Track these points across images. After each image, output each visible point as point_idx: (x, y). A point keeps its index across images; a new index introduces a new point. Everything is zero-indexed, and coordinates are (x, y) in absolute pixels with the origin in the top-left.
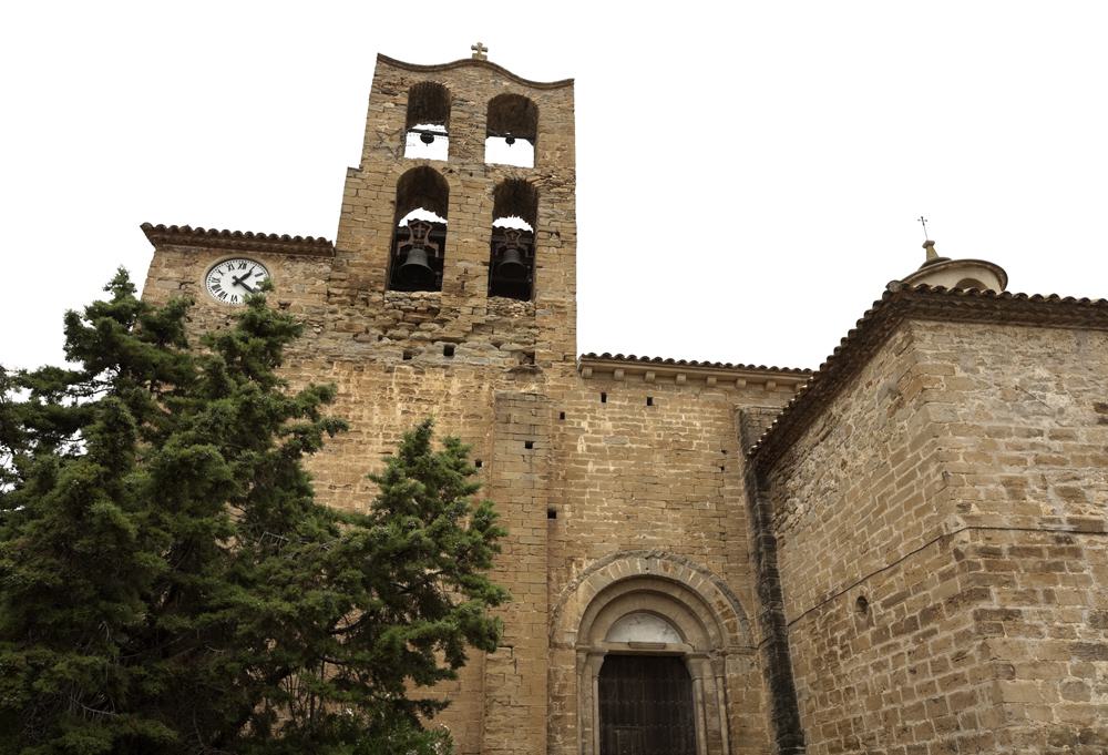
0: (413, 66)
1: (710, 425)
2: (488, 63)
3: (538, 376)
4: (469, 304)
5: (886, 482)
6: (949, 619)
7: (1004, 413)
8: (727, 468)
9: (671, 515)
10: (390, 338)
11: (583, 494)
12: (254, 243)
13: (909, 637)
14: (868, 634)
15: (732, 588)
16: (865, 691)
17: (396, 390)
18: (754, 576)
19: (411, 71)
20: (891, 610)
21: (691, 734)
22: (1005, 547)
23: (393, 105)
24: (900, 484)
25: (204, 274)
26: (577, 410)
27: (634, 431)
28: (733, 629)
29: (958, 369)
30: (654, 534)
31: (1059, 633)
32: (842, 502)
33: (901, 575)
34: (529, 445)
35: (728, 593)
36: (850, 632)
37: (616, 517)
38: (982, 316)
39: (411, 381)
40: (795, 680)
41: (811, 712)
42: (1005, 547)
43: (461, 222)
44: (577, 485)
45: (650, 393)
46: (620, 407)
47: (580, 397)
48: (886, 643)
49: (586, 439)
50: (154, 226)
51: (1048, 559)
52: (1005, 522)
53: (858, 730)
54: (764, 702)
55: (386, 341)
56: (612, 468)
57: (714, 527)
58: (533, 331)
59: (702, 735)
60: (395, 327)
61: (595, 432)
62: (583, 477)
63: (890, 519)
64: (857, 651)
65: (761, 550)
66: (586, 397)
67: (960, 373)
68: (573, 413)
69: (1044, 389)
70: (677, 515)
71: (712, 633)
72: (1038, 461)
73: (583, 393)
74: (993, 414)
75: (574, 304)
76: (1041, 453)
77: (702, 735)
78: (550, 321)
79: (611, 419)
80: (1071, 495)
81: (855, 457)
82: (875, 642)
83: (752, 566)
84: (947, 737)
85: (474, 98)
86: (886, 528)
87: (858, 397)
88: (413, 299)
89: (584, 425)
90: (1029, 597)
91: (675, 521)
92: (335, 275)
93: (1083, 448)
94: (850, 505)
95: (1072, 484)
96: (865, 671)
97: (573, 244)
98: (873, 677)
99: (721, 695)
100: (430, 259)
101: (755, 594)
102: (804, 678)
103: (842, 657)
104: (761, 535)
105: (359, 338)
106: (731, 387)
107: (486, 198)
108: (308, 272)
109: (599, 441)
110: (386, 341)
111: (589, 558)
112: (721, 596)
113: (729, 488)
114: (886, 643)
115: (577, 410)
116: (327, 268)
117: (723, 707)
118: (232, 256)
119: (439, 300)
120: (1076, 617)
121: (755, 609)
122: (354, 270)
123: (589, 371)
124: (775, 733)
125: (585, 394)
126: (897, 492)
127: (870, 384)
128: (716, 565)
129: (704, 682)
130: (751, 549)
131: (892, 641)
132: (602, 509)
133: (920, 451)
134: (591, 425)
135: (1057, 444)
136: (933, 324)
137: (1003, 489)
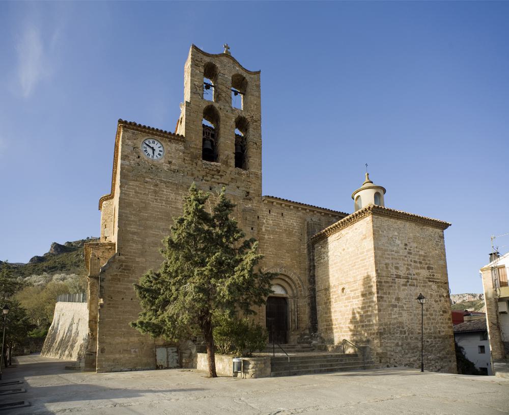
0: (206, 53)
1: (298, 225)
2: (231, 56)
3: (251, 201)
4: (229, 170)
5: (357, 259)
6: (368, 297)
7: (388, 245)
8: (302, 240)
9: (287, 255)
10: (206, 181)
11: (264, 246)
12: (158, 133)
13: (357, 300)
14: (344, 297)
15: (302, 279)
16: (341, 312)
17: (209, 202)
18: (307, 276)
19: (205, 55)
20: (353, 292)
21: (92, 306)
22: (383, 281)
23: (199, 72)
24: (361, 260)
25: (141, 144)
26: (262, 216)
27: (278, 225)
28: (301, 291)
29: (380, 231)
30: (282, 260)
31: (389, 302)
32: (342, 261)
33: (357, 284)
34: (252, 229)
35: (300, 280)
36: (338, 297)
37: (273, 254)
38: (387, 216)
39: (214, 199)
40: (317, 307)
41: (321, 316)
42: (383, 281)
43: (225, 133)
44: (263, 243)
45: (282, 211)
46: (275, 216)
47: (263, 211)
48: (349, 301)
49: (265, 227)
50: (123, 120)
51: (390, 284)
52: (384, 275)
53: (336, 321)
54: (307, 312)
55: (204, 181)
56: (272, 237)
57: (298, 259)
58: (249, 183)
59: (290, 320)
60: (206, 176)
61: (267, 224)
62: (264, 240)
63: (356, 269)
64: (340, 301)
65: (311, 268)
66: (265, 211)
67: (381, 233)
68: (261, 217)
69: (396, 238)
70: (289, 255)
71: (295, 292)
72: (392, 258)
73: (264, 209)
74: (386, 245)
75: (261, 174)
76: (393, 257)
77: (290, 320)
78: (254, 180)
79: (272, 220)
80: (397, 268)
81: (348, 249)
82: (346, 300)
83: (307, 272)
84: (362, 324)
85: (226, 73)
86: (355, 271)
87: (352, 231)
88: (211, 165)
89: (264, 221)
90: (385, 293)
91: (288, 256)
92: (186, 151)
93: (401, 256)
94: (344, 262)
95: (397, 265)
96: (342, 307)
97: (261, 149)
98: (343, 309)
99: (296, 310)
100: (212, 145)
101: (307, 281)
102: (320, 307)
103: (335, 302)
104: (312, 264)
105: (195, 179)
106: (304, 212)
107: (232, 122)
108: (177, 148)
109: (268, 227)
110: (204, 181)
111: (266, 267)
112: (299, 282)
113: (302, 247)
114: (349, 301)
115: (262, 216)
116: (182, 148)
117: (296, 313)
118: (150, 137)
119: (220, 167)
120: (393, 298)
121: (307, 285)
122: (192, 150)
123: (266, 202)
124: (310, 321)
125: (264, 208)
126: (360, 262)
127: (356, 229)
128: (297, 271)
129: (291, 305)
130: (307, 267)
131: (351, 300)
132: (269, 251)
133: (368, 253)
134: (266, 221)
135: (396, 254)
136: (377, 217)
137: (385, 266)
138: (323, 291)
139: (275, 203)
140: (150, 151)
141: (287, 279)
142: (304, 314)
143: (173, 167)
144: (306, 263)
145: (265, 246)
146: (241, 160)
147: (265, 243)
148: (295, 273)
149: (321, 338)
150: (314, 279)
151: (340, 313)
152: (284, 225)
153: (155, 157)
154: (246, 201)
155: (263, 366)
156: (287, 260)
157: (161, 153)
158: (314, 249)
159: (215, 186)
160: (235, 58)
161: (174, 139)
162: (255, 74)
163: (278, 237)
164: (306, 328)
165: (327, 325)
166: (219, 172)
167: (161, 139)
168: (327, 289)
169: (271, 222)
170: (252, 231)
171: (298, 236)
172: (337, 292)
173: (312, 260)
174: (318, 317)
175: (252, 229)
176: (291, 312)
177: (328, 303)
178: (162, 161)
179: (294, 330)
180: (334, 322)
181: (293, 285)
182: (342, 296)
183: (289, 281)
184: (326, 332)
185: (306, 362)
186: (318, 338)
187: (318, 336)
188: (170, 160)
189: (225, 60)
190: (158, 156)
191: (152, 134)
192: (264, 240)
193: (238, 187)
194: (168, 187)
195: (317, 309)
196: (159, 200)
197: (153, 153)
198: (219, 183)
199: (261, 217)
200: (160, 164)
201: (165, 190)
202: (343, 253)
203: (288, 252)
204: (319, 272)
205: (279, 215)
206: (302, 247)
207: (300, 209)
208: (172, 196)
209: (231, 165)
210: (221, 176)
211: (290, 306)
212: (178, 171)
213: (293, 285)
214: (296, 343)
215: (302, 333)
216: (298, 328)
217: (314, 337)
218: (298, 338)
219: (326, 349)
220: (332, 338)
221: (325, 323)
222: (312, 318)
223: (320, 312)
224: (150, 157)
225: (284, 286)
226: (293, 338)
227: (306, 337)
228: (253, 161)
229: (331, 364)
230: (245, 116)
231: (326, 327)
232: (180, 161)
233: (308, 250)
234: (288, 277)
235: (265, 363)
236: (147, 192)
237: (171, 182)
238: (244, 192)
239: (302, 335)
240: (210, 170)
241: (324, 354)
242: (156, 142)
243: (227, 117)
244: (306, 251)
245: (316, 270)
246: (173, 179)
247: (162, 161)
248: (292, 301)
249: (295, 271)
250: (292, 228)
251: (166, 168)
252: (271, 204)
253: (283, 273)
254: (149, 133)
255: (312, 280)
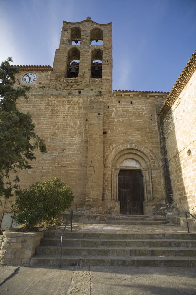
3: (102, 97)
8: (152, 119)
9: (137, 132)
15: (154, 151)
18: (160, 148)
19: (72, 24)
26: (112, 105)
27: (127, 110)
28: (154, 163)
30: (132, 137)
34: (99, 114)
35: (153, 153)
40: (171, 176)
41: (174, 185)
46: (124, 104)
47: (113, 102)
49: (115, 113)
56: (121, 120)
58: (101, 86)
60: (67, 87)
62: (114, 123)
70: (139, 132)
71: (148, 164)
79: (121, 107)
88: (71, 80)
89: (114, 109)
91: (138, 134)
92: (52, 75)
99: (151, 181)
101: (160, 153)
102: (173, 175)
106: (153, 98)
109: (118, 113)
111: (115, 144)
112: (151, 154)
113: (153, 125)
115: (112, 105)
116: (50, 73)
117: (151, 184)
119: (77, 79)
122: (57, 74)
123: (115, 95)
124: (165, 191)
128: (149, 146)
129: (146, 177)
130: (159, 141)
134: (116, 109)
138: (173, 159)
139: (123, 95)
140: (28, 79)
141: (139, 153)
142: (159, 184)
143: (41, 85)
144: (158, 138)
145: (115, 128)
146: (96, 72)
147: (114, 125)
148: (146, 147)
149: (177, 209)
150: (164, 149)
151: (190, 179)
152: (133, 110)
153: (31, 82)
154: (98, 97)
155: (19, 246)
156: (137, 136)
157: (35, 79)
158: (163, 124)
159: (73, 91)
160: (93, 20)
161: (45, 70)
162: (108, 25)
163: (127, 119)
164: (162, 199)
165: (180, 195)
166: (76, 83)
167: (36, 72)
168: (176, 155)
169: (121, 109)
170: (98, 115)
171: (148, 117)
172: (184, 157)
173: (162, 133)
174: (172, 187)
175: (99, 114)
176: (146, 183)
177: (179, 169)
178: (35, 83)
179: (149, 201)
180: (187, 191)
181: (146, 158)
182: (189, 159)
183: (141, 155)
184: (180, 202)
185: (112, 244)
186: (175, 209)
187: (173, 207)
188: (40, 82)
189: (86, 24)
190: (33, 81)
191: (31, 70)
192: (114, 123)
193: (92, 90)
194: (36, 97)
195: (171, 178)
196: (28, 106)
197: (30, 80)
198: (76, 90)
199: (111, 106)
200: (33, 86)
201: (33, 100)
202: (183, 114)
203: (138, 130)
204: (168, 143)
205: (128, 103)
206: (153, 125)
207: (148, 96)
208: (38, 102)
209: (87, 77)
210: (78, 85)
211: (145, 177)
212: (45, 87)
213: (146, 158)
214: (151, 214)
215: (158, 203)
216: (153, 199)
217: (170, 208)
218: (154, 209)
219: (177, 223)
220: (187, 209)
221: (178, 193)
222: (166, 188)
223: (173, 181)
224: (28, 82)
225: (138, 160)
226: (149, 208)
227: (162, 208)
228: (105, 72)
229: (152, 251)
230: (99, 48)
231: (179, 197)
232: (47, 81)
233: (158, 126)
234: (140, 151)
235: (23, 242)
236: (21, 103)
237: (39, 94)
238: (97, 92)
239: (158, 207)
240: (70, 83)
241: (171, 230)
242: (33, 74)
243: (85, 51)
244: (157, 128)
245: (166, 141)
246: (41, 92)
247: (35, 83)
248: (147, 173)
249: (146, 145)
250: (141, 112)
251: (36, 87)
252: (120, 96)
253: (134, 147)
254: (28, 70)
255: (164, 152)
